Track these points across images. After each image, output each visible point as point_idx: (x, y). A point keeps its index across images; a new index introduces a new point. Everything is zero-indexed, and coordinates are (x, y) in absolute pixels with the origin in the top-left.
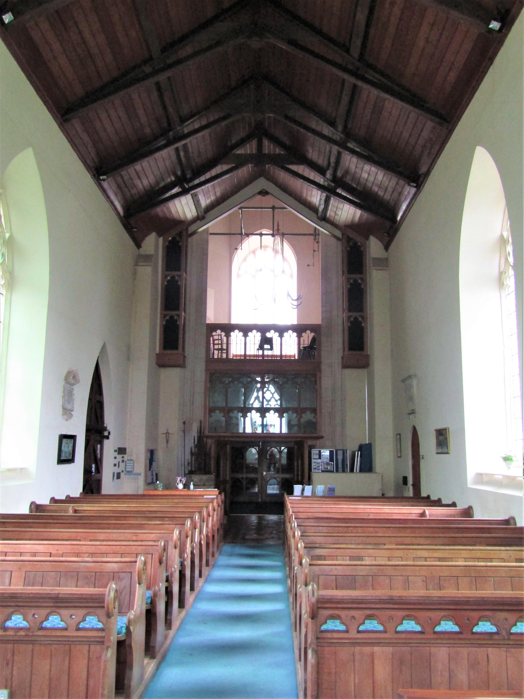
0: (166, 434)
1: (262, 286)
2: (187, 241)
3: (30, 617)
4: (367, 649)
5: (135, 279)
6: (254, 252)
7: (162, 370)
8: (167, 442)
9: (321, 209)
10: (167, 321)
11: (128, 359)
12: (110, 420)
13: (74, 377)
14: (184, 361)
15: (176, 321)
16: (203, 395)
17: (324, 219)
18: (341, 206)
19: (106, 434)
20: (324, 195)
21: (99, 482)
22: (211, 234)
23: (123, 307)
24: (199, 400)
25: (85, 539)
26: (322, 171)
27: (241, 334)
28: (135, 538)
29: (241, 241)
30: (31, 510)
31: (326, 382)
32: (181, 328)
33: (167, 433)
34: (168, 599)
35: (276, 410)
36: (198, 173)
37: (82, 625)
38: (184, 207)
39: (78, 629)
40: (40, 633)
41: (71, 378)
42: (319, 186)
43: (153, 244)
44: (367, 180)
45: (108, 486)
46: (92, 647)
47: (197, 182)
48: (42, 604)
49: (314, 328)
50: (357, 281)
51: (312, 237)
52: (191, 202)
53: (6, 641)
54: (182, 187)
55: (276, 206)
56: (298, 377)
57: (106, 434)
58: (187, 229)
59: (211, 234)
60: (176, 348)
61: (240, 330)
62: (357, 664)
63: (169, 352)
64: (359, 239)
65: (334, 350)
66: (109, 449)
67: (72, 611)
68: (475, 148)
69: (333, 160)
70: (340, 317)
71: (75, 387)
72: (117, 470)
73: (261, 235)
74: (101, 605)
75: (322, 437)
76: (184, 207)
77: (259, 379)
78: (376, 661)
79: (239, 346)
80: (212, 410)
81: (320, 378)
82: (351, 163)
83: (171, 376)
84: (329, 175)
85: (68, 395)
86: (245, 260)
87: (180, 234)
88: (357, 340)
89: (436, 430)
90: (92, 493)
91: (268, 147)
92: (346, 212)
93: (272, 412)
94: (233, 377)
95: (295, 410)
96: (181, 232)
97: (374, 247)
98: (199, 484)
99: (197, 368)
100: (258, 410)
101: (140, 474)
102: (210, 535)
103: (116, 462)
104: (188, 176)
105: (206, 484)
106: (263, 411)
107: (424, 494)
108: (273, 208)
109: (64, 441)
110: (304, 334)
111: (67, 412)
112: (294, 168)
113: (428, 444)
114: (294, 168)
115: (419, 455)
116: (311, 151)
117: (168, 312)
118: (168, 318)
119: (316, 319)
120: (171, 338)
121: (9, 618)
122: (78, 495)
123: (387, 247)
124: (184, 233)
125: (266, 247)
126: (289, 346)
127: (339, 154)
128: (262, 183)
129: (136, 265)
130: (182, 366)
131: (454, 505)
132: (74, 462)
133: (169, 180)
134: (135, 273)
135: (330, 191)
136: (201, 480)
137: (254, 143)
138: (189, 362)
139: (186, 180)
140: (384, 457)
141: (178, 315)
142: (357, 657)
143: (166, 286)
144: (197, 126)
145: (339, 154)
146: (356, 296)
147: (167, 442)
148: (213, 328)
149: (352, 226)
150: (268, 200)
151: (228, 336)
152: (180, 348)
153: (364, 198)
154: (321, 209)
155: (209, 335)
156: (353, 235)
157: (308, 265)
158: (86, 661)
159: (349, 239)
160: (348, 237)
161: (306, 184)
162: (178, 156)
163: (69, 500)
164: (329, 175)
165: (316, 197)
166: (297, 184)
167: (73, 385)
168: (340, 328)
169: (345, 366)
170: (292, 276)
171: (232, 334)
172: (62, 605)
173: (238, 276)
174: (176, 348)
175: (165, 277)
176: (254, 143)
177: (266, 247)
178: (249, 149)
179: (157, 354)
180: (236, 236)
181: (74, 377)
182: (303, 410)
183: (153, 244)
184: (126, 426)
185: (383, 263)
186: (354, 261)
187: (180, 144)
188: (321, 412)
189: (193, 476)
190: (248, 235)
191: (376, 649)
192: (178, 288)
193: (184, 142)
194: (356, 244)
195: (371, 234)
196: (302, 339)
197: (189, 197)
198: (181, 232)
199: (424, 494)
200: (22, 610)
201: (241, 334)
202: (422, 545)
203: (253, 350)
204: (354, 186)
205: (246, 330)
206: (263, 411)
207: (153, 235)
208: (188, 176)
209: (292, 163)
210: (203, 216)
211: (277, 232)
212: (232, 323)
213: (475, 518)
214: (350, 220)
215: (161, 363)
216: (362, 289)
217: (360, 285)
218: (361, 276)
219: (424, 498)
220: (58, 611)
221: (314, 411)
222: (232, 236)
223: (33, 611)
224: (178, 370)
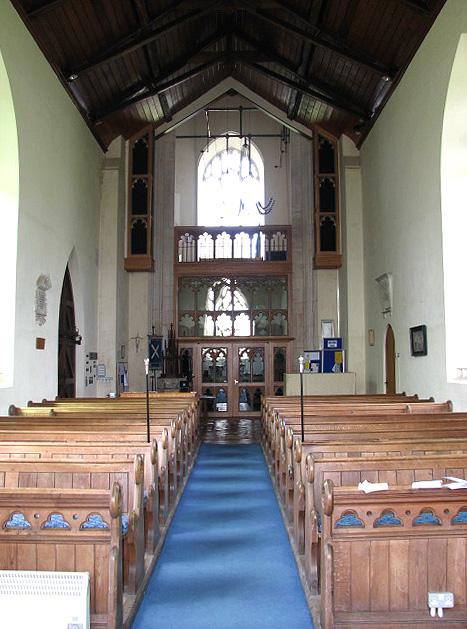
1: (229, 190)
2: (154, 144)
3: (32, 518)
4: (384, 543)
5: (102, 183)
6: (219, 155)
7: (130, 275)
8: (137, 346)
9: (291, 107)
11: (97, 265)
12: (80, 325)
13: (46, 282)
14: (153, 265)
15: (145, 221)
16: (172, 299)
17: (293, 116)
18: (312, 103)
19: (77, 339)
20: (296, 92)
21: (73, 386)
22: (178, 137)
23: (89, 215)
24: (169, 304)
25: (72, 440)
26: (294, 68)
27: (229, 236)
28: (122, 439)
29: (208, 144)
30: (10, 414)
31: (297, 283)
32: (149, 231)
35: (246, 312)
36: (164, 75)
37: (86, 525)
38: (151, 109)
39: (82, 528)
40: (44, 533)
41: (43, 284)
42: (291, 83)
43: (119, 147)
44: (340, 76)
45: (80, 389)
46: (98, 547)
47: (165, 81)
48: (44, 505)
49: (286, 230)
52: (158, 104)
53: (6, 540)
54: (149, 86)
55: (243, 106)
56: (264, 281)
57: (77, 339)
58: (154, 132)
59: (178, 137)
60: (145, 252)
62: (372, 558)
64: (330, 138)
65: (305, 250)
66: (80, 352)
67: (74, 512)
68: (225, 78)
69: (306, 55)
70: (309, 218)
71: (46, 292)
72: (89, 375)
73: (227, 136)
74: (105, 505)
75: (293, 339)
76: (151, 109)
77: (229, 282)
78: (392, 555)
79: (205, 249)
80: (181, 315)
81: (291, 281)
82: (325, 56)
83: (139, 282)
84: (301, 71)
85: (41, 301)
86: (211, 162)
87: (146, 137)
88: (328, 239)
89: (43, 348)
90: (67, 397)
91: (238, 44)
92: (318, 110)
93: (242, 314)
94: (198, 278)
95: (266, 313)
96: (148, 134)
97: (347, 146)
99: (166, 275)
100: (228, 313)
101: (111, 379)
102: (191, 436)
103: (88, 366)
104: (156, 76)
106: (233, 314)
107: (399, 391)
108: (241, 108)
109: (416, 334)
111: (41, 316)
112: (265, 65)
113: (403, 345)
114: (265, 65)
115: (394, 355)
116: (282, 47)
117: (136, 216)
118: (135, 221)
119: (281, 220)
120: (139, 241)
121: (10, 518)
122: (54, 399)
123: (359, 146)
124: (151, 135)
125: (233, 149)
126: (246, 248)
127: (313, 47)
128: (230, 83)
129: (103, 168)
130: (151, 270)
131: (431, 400)
132: (426, 354)
133: (136, 80)
134: (101, 178)
135: (301, 88)
137: (223, 41)
138: (157, 266)
139: (153, 84)
140: (357, 354)
141: (146, 219)
142: (373, 551)
144: (165, 21)
145: (313, 47)
146: (328, 198)
148: (180, 231)
149: (323, 123)
150: (236, 101)
151: (196, 239)
152: (149, 252)
153: (334, 93)
154: (291, 107)
156: (325, 134)
158: (92, 560)
159: (320, 138)
160: (319, 135)
161: (276, 82)
162: (146, 52)
163: (45, 403)
164: (301, 71)
165: (287, 95)
166: (267, 81)
167: (45, 290)
168: (310, 229)
170: (258, 178)
171: (200, 236)
172: (65, 505)
173: (204, 179)
174: (145, 252)
175: (131, 180)
176: (223, 41)
177: (233, 149)
178: (219, 46)
179: (125, 260)
180: (201, 139)
181: (46, 282)
182: (275, 313)
183: (119, 147)
184: (99, 332)
185: (356, 162)
186: (326, 161)
187: (148, 41)
188: (292, 314)
190: (214, 137)
191: (393, 542)
192: (146, 191)
193: (151, 40)
194: (326, 142)
195: (344, 132)
196: (272, 241)
197: (156, 97)
198: (148, 134)
199: (399, 391)
200: (22, 511)
201: (247, 235)
202: (416, 439)
203: (223, 252)
204: (327, 81)
205: (215, 233)
206: (233, 314)
207: (120, 138)
208: (156, 76)
209: (261, 61)
210: (167, 118)
212: (199, 225)
213: (454, 411)
214: (321, 118)
215: (129, 268)
216: (333, 188)
219: (400, 395)
220: (60, 511)
221: (285, 313)
223: (34, 512)
224: (146, 274)
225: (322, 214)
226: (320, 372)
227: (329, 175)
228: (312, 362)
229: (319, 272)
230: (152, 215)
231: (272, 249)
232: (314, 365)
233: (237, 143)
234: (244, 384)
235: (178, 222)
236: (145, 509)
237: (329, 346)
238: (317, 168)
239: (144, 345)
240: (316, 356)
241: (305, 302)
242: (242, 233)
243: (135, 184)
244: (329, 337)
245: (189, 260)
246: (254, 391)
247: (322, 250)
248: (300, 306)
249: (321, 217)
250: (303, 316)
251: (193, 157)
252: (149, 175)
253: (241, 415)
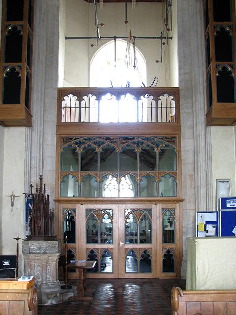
0: (11, 196)
8: (12, 205)
10: (8, 74)
33: (13, 196)
34: (148, 183)
50: (225, 29)
51: (160, 40)
61: (93, 94)
63: (175, 268)
75: (182, 201)
98: (38, 252)
105: (47, 252)
110: (161, 97)
136: (40, 247)
138: (36, 119)
141: (20, 67)
143: (7, 37)
147: (12, 205)
148: (63, 93)
155: (60, 99)
157: (157, 61)
169: (211, 121)
174: (18, 102)
189: (30, 242)
211: (131, 39)
217: (228, 32)
218: (229, 23)
222: (90, 40)
224: (23, 130)
225: (219, 63)
226: (217, 234)
227: (225, 23)
228: (207, 223)
229: (214, 129)
230: (29, 63)
231: (160, 120)
232: (209, 227)
233: (121, 44)
234: (131, 246)
235: (61, 84)
236: (175, 180)
237: (228, 205)
238: (211, 15)
239: (20, 204)
240: (212, 217)
241: (195, 163)
242: (128, 95)
243: (9, 32)
244: (226, 196)
245: (73, 121)
246: (141, 253)
247: (219, 101)
248: (190, 167)
249: (217, 67)
250: (194, 176)
251: (87, 60)
252: (25, 22)
253: (127, 276)
